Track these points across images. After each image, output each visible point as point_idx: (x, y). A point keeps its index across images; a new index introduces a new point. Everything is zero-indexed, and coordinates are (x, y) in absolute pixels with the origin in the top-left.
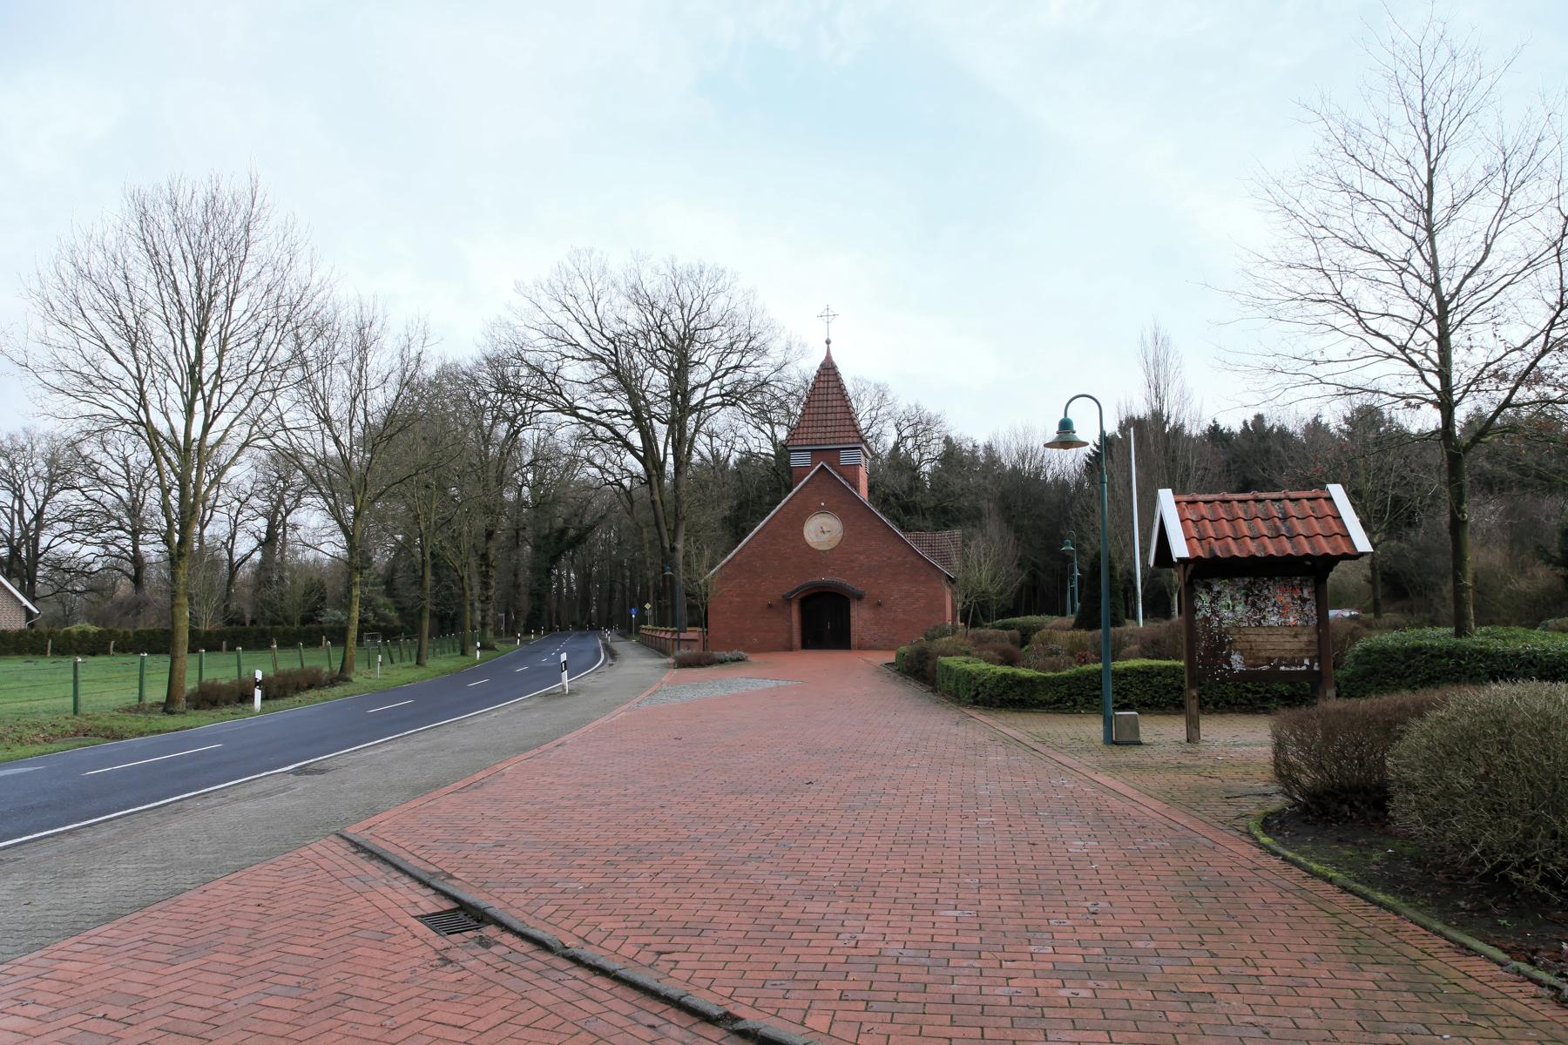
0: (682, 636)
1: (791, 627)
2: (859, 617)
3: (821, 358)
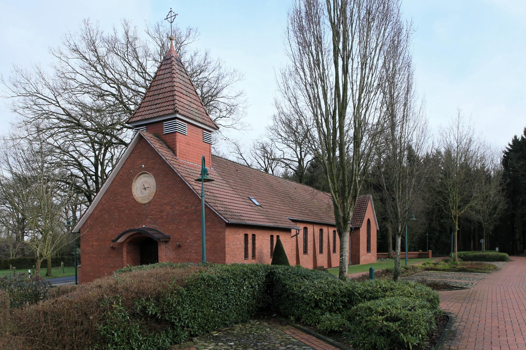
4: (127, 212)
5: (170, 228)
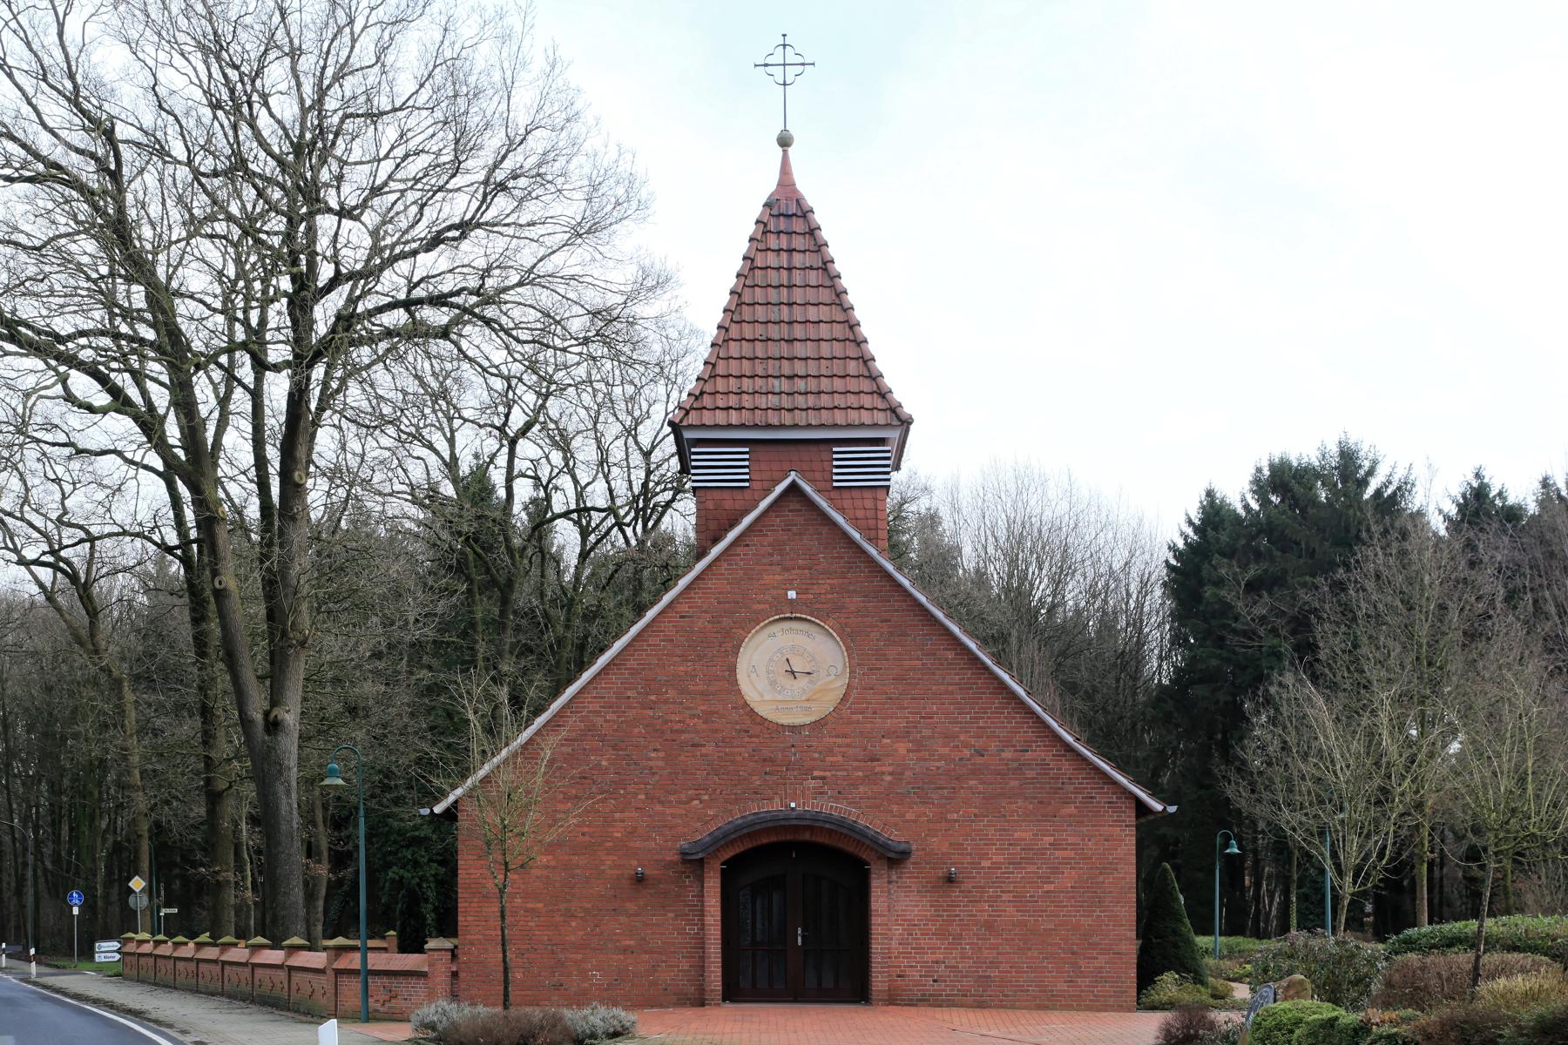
0: (353, 961)
1: (701, 945)
2: (896, 913)
3: (767, 185)
4: (709, 749)
5: (910, 816)
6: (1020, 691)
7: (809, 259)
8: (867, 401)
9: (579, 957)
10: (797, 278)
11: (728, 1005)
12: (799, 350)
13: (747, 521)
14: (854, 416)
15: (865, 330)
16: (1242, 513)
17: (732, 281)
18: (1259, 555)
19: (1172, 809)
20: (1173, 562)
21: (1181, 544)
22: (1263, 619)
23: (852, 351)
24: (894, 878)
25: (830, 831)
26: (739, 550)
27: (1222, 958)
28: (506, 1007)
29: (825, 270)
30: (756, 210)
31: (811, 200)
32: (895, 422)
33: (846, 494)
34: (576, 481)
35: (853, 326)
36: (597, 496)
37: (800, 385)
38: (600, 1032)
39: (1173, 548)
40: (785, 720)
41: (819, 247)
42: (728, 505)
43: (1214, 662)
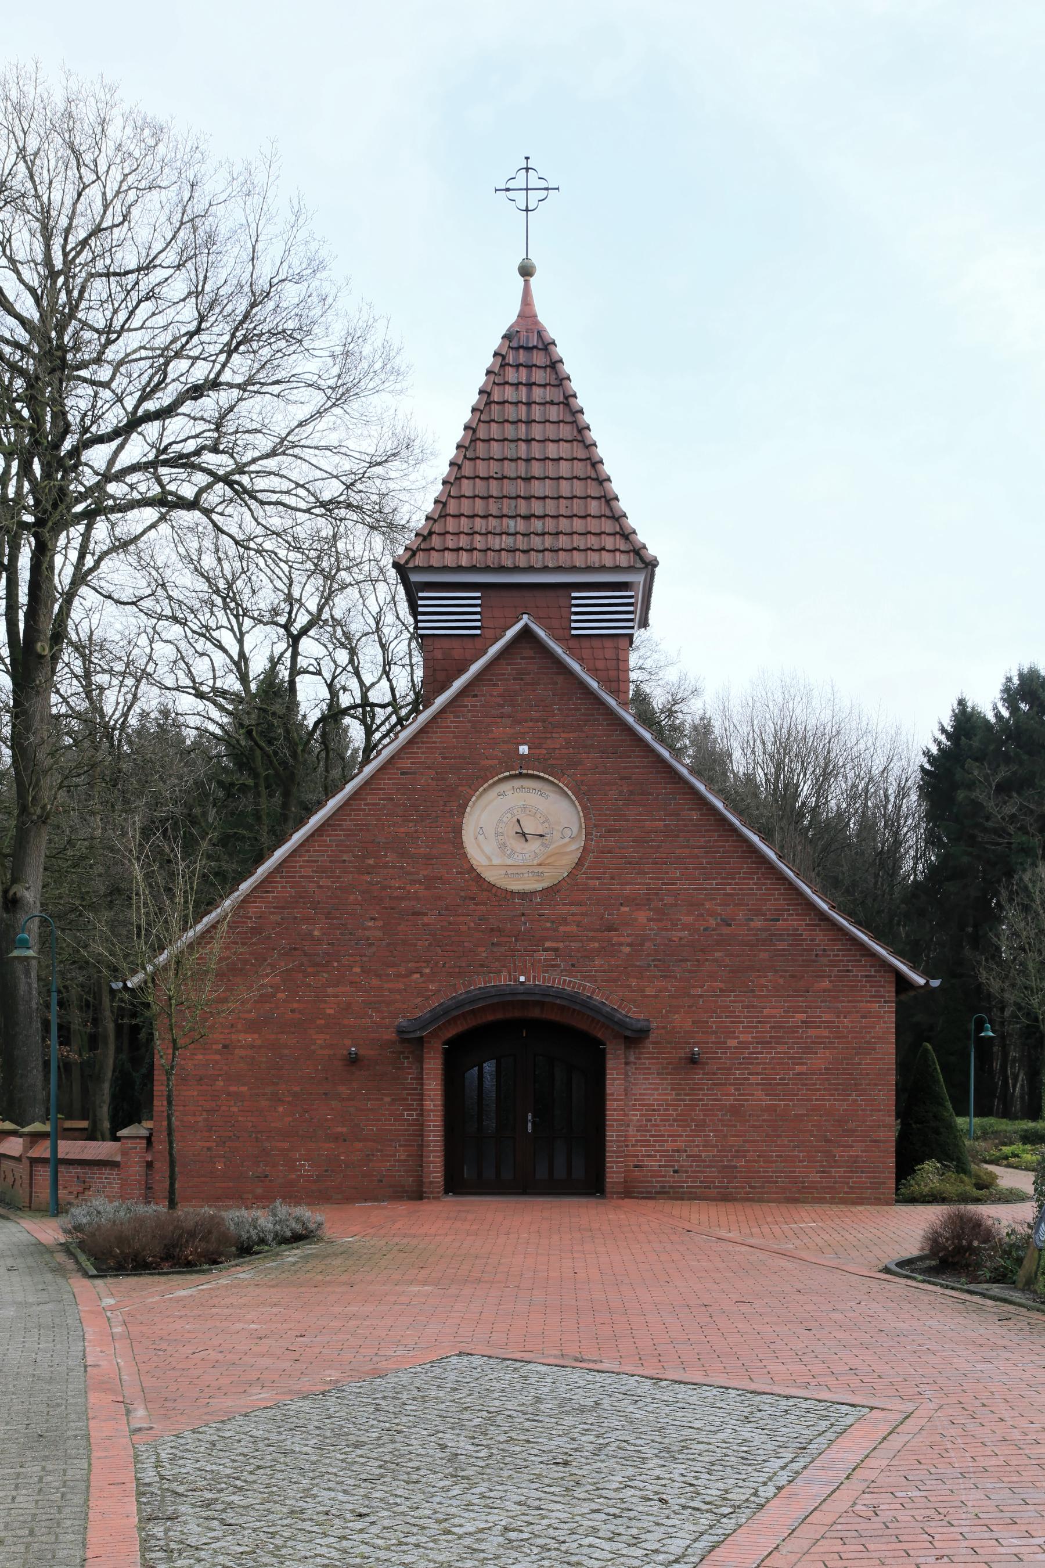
1: (419, 1129)
2: (635, 1100)
3: (508, 317)
4: (431, 917)
5: (649, 991)
6: (771, 854)
7: (549, 394)
8: (609, 542)
9: (287, 1145)
10: (537, 413)
11: (450, 1198)
12: (537, 488)
13: (475, 668)
14: (594, 558)
15: (608, 468)
16: (993, 720)
17: (466, 416)
18: (1007, 759)
19: (936, 983)
20: (927, 766)
21: (934, 750)
22: (1013, 818)
23: (593, 490)
24: (632, 1059)
25: (562, 1008)
26: (467, 701)
27: (977, 1139)
28: (172, 1204)
29: (567, 405)
30: (495, 342)
31: (553, 332)
32: (639, 565)
33: (585, 643)
34: (361, 683)
35: (596, 463)
36: (380, 694)
37: (537, 525)
38: (270, 1237)
39: (927, 753)
40: (515, 886)
41: (561, 381)
42: (457, 654)
43: (965, 859)
